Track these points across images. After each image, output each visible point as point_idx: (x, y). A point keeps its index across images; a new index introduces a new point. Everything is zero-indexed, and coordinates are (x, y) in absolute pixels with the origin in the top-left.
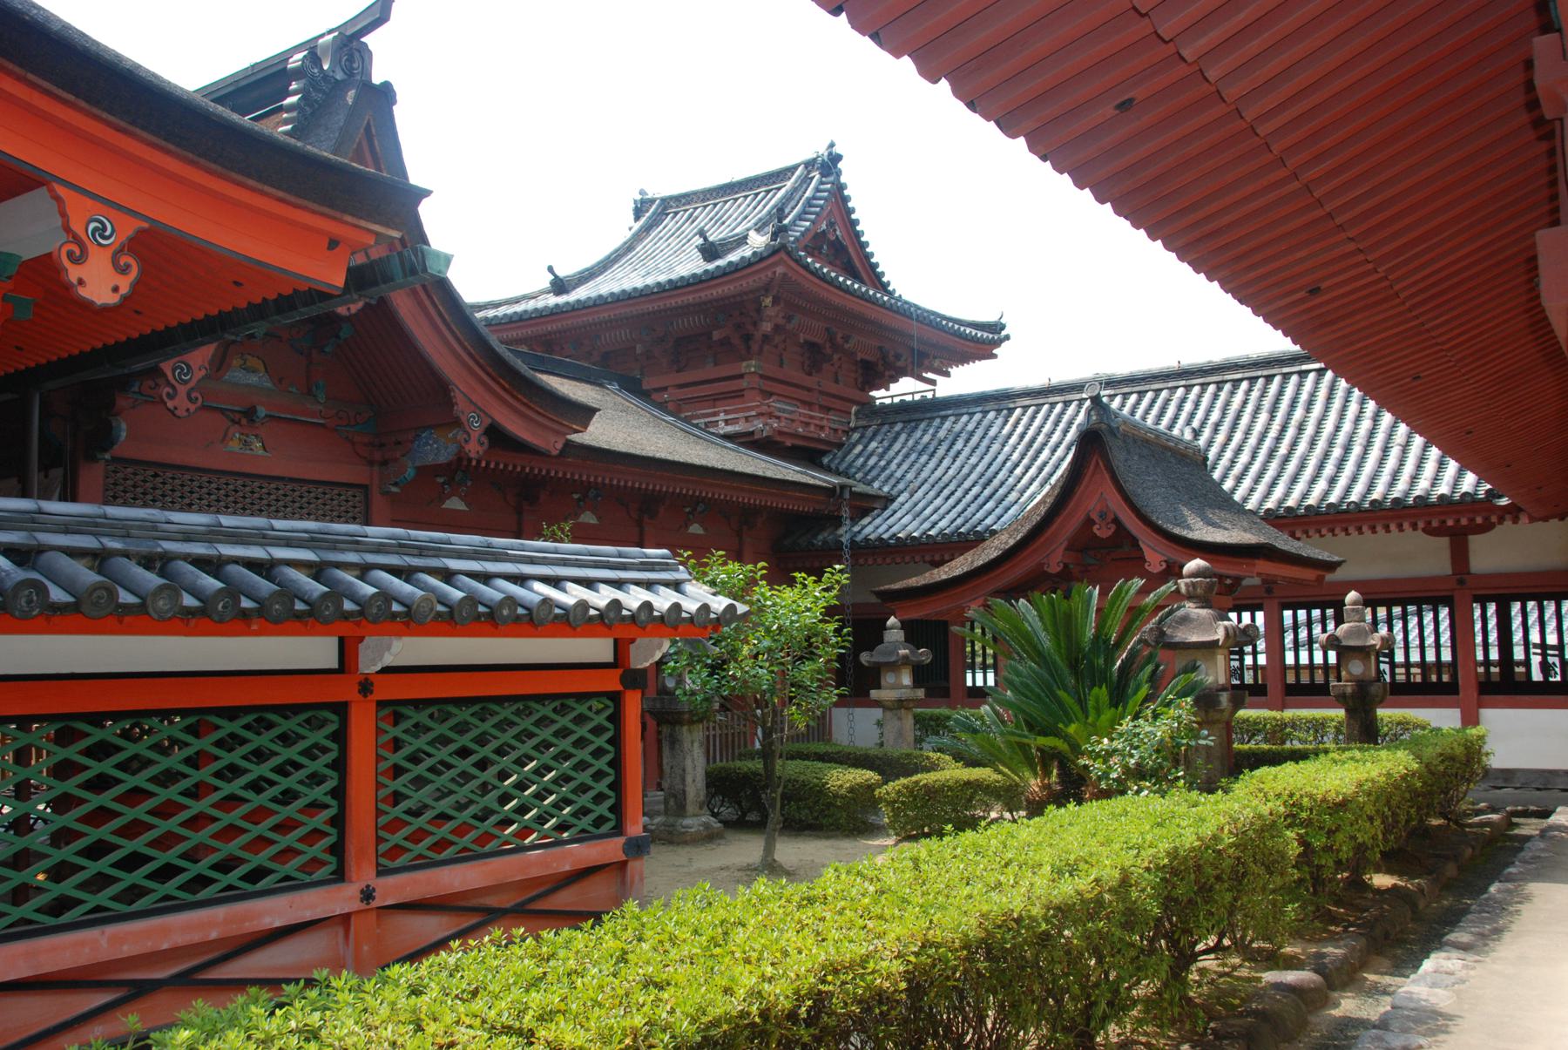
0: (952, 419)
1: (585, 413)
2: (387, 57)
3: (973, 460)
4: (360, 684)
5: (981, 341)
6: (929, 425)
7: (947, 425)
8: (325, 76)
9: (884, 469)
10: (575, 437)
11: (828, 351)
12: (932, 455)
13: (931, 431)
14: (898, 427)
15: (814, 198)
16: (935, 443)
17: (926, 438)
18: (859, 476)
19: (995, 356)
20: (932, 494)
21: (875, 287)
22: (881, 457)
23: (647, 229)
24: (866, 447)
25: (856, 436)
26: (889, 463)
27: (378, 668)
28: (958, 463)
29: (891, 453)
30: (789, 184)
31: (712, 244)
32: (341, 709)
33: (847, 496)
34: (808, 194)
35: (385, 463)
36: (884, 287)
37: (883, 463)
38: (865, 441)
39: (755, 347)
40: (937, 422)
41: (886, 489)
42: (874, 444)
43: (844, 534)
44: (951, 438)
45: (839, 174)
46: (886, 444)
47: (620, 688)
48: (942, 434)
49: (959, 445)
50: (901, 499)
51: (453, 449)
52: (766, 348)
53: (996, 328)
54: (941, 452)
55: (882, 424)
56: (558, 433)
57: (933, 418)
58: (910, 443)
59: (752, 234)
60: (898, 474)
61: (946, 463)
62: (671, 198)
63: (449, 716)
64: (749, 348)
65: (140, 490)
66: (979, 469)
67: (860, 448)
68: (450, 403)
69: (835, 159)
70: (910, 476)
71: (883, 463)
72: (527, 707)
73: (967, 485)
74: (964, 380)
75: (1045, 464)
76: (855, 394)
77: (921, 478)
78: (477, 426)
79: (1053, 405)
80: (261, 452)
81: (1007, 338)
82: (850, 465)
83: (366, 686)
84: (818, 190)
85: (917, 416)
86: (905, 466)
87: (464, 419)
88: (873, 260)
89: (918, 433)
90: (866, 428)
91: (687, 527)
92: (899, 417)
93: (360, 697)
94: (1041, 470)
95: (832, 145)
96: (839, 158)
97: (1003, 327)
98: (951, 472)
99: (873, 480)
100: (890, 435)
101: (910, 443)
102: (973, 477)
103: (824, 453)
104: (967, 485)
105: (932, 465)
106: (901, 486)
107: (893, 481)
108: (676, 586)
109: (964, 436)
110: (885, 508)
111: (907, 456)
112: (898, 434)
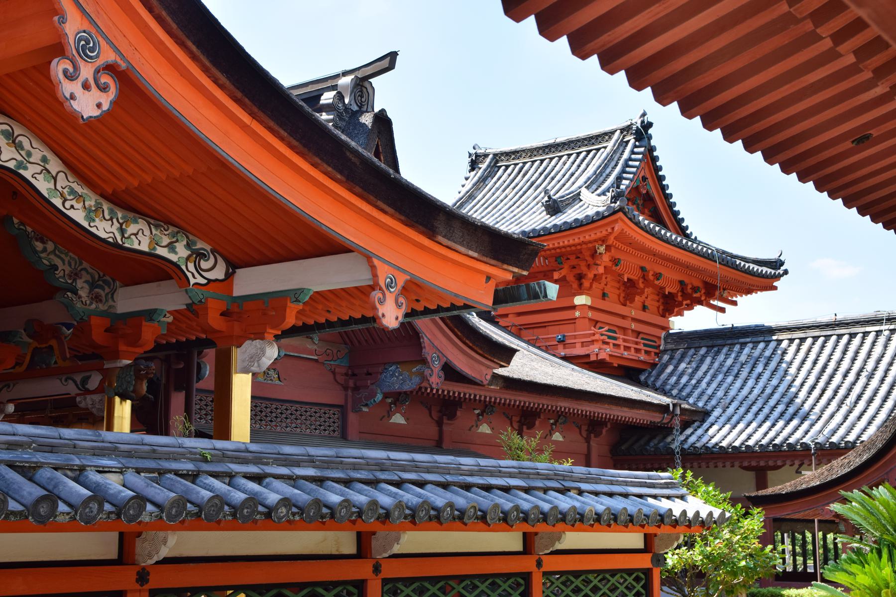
0: (751, 345)
1: (507, 354)
2: (386, 94)
3: (774, 382)
4: (138, 573)
5: (764, 275)
6: (730, 350)
7: (747, 350)
8: (346, 108)
9: (695, 387)
10: (501, 371)
11: (641, 285)
12: (736, 376)
13: (733, 355)
14: (703, 351)
15: (630, 159)
16: (738, 366)
17: (729, 362)
18: (675, 392)
19: (775, 288)
20: (742, 410)
21: (678, 233)
22: (692, 376)
23: (483, 180)
24: (676, 367)
25: (666, 357)
26: (699, 382)
27: (156, 559)
28: (761, 384)
29: (700, 373)
30: (610, 145)
31: (555, 201)
32: (527, 577)
33: (678, 411)
34: (626, 155)
35: (356, 389)
36: (682, 231)
37: (694, 382)
38: (674, 362)
39: (586, 284)
40: (737, 348)
41: (700, 404)
42: (683, 366)
43: (676, 441)
44: (752, 362)
45: (650, 138)
46: (694, 365)
47: (650, 566)
48: (743, 358)
49: (759, 368)
50: (716, 413)
51: (416, 380)
52: (595, 285)
53: (776, 264)
54: (744, 374)
55: (689, 348)
56: (488, 367)
57: (734, 344)
58: (716, 365)
59: (585, 194)
60: (709, 391)
61: (750, 383)
62: (502, 154)
63: (475, 587)
64: (580, 285)
65: (204, 412)
66: (781, 389)
67: (670, 368)
68: (419, 346)
69: (648, 126)
70: (720, 394)
71: (694, 382)
72: (568, 580)
73: (772, 402)
74: (747, 310)
75: (839, 387)
76: (659, 320)
77: (730, 397)
78: (437, 366)
79: (840, 336)
80: (278, 382)
81: (786, 272)
82: (665, 382)
83: (143, 576)
84: (633, 153)
85: (720, 342)
86: (714, 385)
87: (429, 359)
88: (676, 209)
89: (721, 357)
90: (674, 351)
91: (390, 417)
92: (703, 342)
93: (373, 576)
94: (836, 392)
95: (644, 115)
96: (650, 125)
97: (782, 264)
98: (756, 391)
99: (689, 395)
100: (698, 358)
101: (716, 365)
102: (776, 396)
103: (641, 371)
104: (772, 402)
105: (738, 384)
106: (714, 402)
107: (705, 398)
108: (682, 497)
109: (763, 361)
110: (703, 421)
111: (714, 376)
112: (704, 357)
